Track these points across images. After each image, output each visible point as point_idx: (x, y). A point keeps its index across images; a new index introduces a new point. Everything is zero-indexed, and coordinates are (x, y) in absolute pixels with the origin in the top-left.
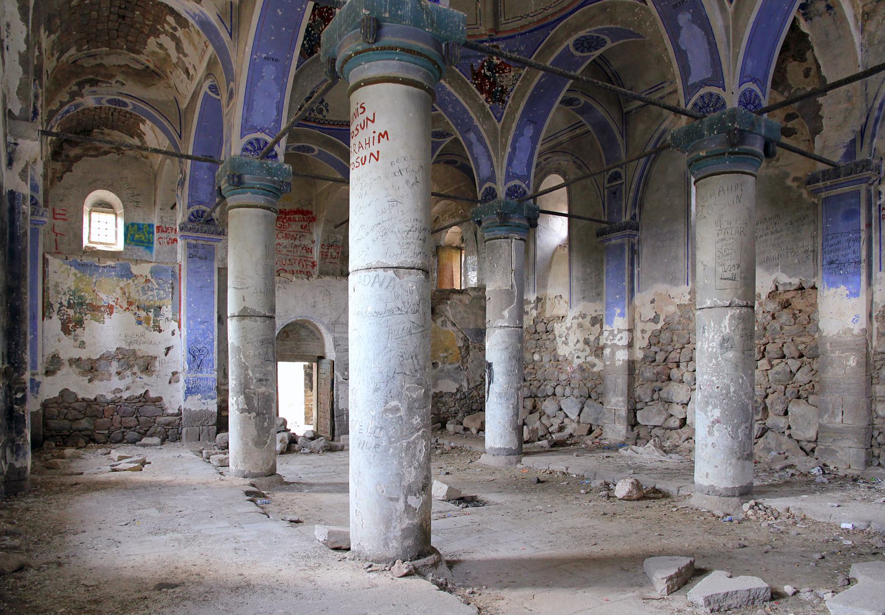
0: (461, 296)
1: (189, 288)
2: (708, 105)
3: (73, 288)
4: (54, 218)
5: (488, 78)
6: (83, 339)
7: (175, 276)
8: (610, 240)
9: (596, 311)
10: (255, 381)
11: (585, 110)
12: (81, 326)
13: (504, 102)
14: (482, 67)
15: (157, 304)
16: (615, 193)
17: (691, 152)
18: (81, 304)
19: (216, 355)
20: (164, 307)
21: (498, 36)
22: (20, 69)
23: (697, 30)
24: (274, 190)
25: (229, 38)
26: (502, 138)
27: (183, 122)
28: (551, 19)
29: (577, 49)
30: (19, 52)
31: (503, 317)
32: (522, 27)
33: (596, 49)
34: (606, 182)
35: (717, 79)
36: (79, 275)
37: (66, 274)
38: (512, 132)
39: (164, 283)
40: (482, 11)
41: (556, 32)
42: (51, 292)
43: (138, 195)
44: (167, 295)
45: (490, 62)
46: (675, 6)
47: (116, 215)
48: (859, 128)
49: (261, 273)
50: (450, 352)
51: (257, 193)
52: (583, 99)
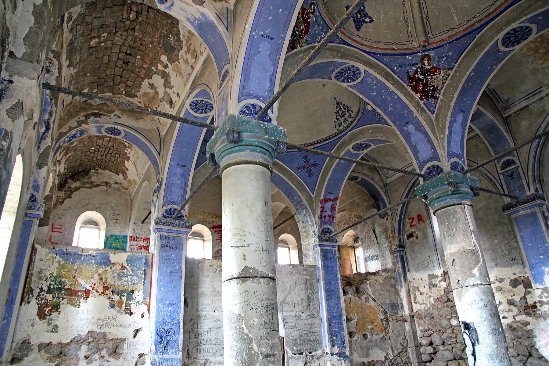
0: (376, 277)
1: (160, 273)
3: (55, 275)
4: (52, 231)
5: (421, 80)
6: (57, 323)
7: (148, 264)
8: (519, 211)
9: (514, 274)
10: (261, 357)
12: (57, 310)
13: (435, 98)
14: (416, 72)
15: (131, 288)
16: (511, 176)
18: (60, 289)
19: (181, 336)
20: (136, 292)
21: (429, 47)
22: (32, 20)
24: (270, 150)
25: (225, 30)
26: (438, 125)
27: (162, 144)
30: (34, 4)
31: (473, 276)
32: (450, 37)
36: (62, 263)
37: (51, 261)
38: (449, 118)
39: (138, 270)
41: (482, 35)
42: (34, 278)
43: (118, 214)
44: (140, 281)
45: (423, 68)
47: (100, 229)
49: (262, 228)
50: (375, 324)
51: (255, 151)
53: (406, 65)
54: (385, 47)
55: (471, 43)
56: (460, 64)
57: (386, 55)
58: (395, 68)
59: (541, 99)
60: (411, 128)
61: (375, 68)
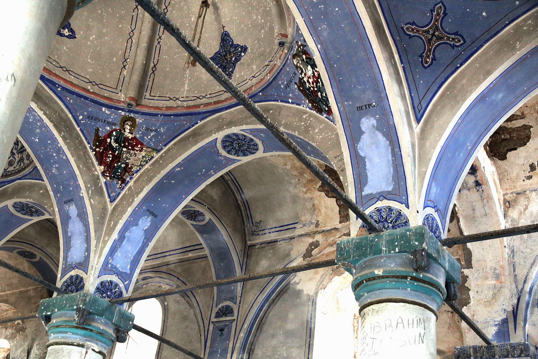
2: (386, 220)
5: (113, 150)
11: (207, 230)
13: (124, 181)
14: (110, 135)
16: (222, 330)
17: (362, 269)
21: (138, 109)
23: (380, 136)
26: (110, 220)
28: (202, 109)
29: (224, 147)
32: (168, 108)
33: (245, 155)
34: (213, 315)
35: (400, 192)
38: (125, 217)
40: (126, 79)
41: (204, 124)
46: (360, 108)
48: (510, 309)
52: (208, 216)
53: (97, 119)
54: (75, 81)
55: (190, 128)
56: (169, 149)
57: (73, 93)
58: (81, 117)
59: (291, 239)
60: (73, 210)
61: (46, 104)
